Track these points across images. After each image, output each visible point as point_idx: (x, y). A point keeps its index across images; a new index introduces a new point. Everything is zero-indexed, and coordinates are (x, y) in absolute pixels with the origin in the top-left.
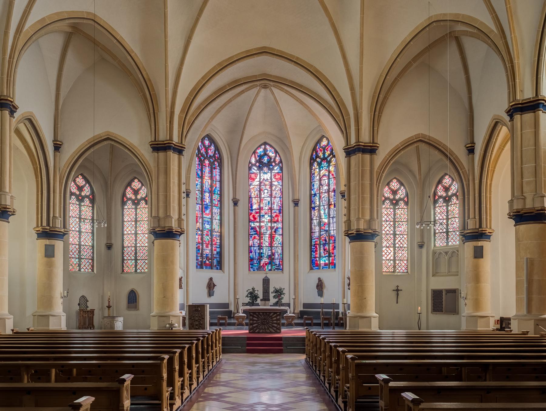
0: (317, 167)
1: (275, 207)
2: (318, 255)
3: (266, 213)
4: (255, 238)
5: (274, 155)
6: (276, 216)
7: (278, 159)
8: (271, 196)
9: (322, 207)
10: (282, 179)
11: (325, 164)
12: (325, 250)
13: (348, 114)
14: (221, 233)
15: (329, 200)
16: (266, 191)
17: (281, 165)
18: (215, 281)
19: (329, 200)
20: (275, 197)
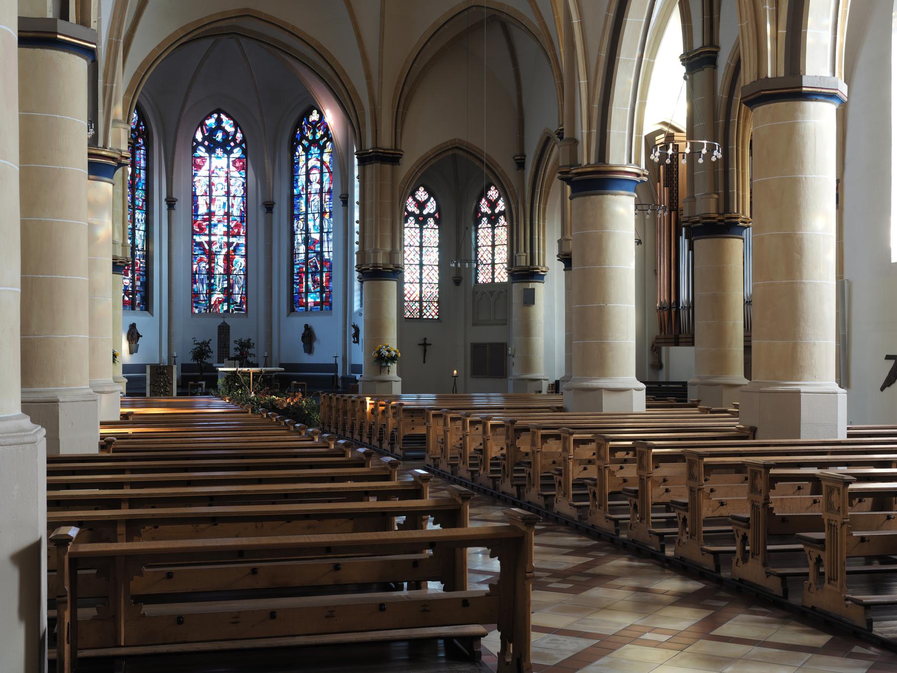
0: (303, 153)
1: (236, 212)
2: (304, 290)
3: (219, 221)
4: (201, 260)
5: (233, 129)
6: (236, 226)
7: (239, 136)
8: (228, 193)
9: (310, 216)
10: (245, 168)
11: (315, 150)
12: (314, 281)
13: (362, 108)
14: (147, 251)
15: (322, 205)
16: (220, 186)
17: (244, 145)
18: (139, 329)
19: (322, 205)
20: (234, 196)
